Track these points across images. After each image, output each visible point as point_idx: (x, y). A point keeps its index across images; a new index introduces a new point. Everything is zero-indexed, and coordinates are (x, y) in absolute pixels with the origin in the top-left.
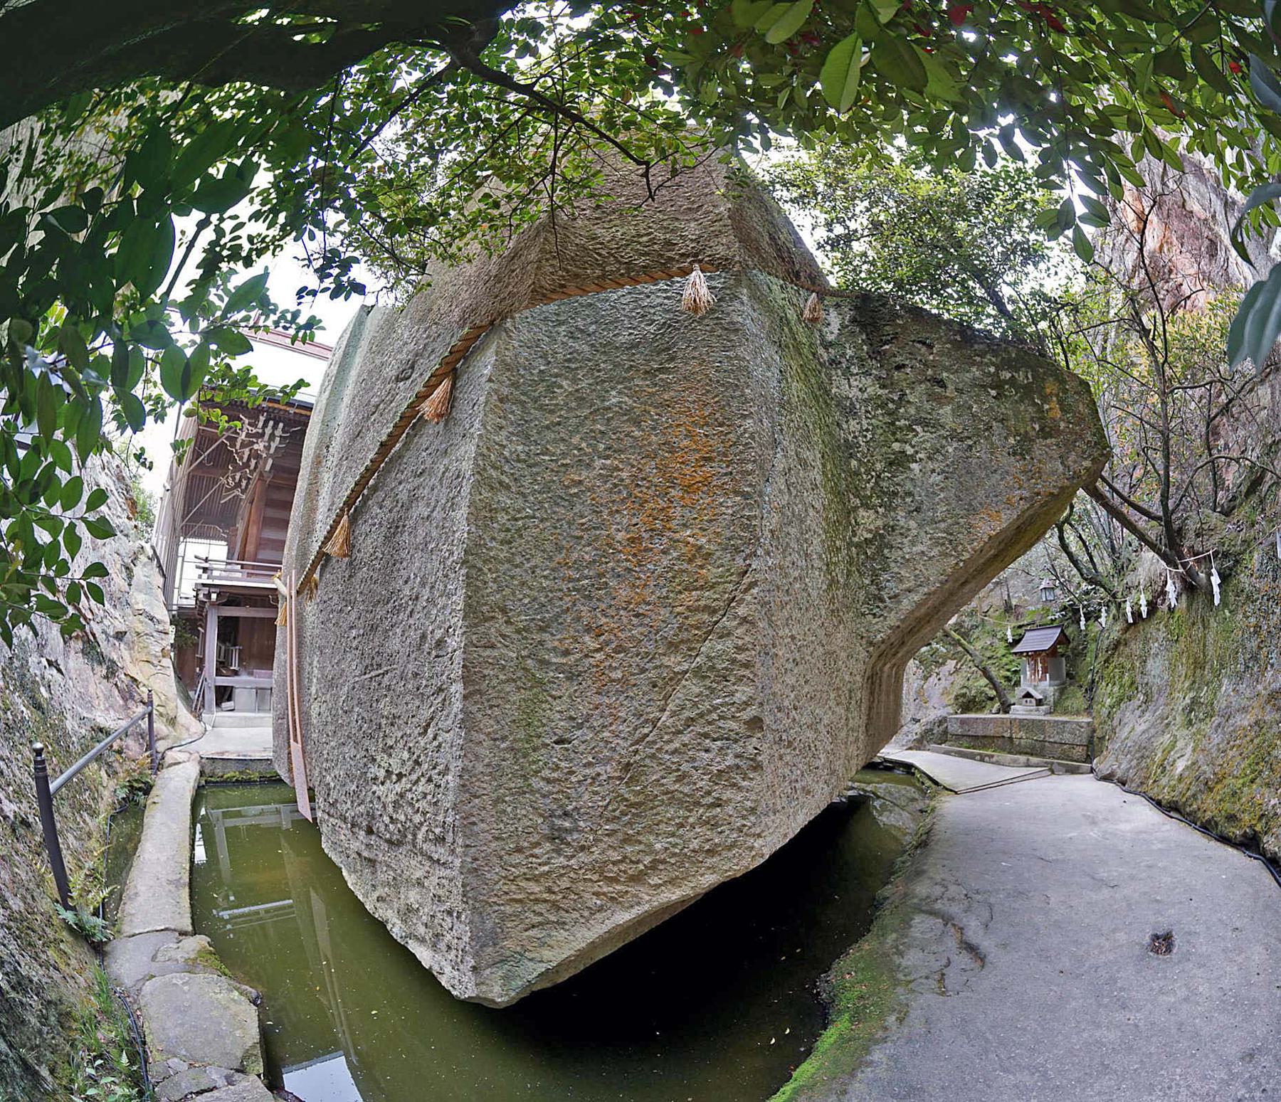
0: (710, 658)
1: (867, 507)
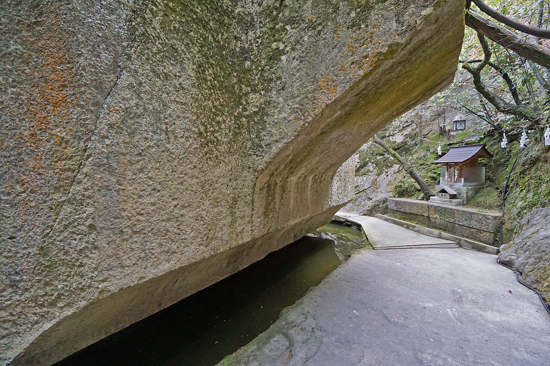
0: (73, 194)
1: (254, 91)
